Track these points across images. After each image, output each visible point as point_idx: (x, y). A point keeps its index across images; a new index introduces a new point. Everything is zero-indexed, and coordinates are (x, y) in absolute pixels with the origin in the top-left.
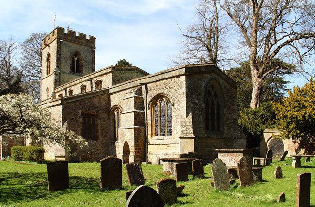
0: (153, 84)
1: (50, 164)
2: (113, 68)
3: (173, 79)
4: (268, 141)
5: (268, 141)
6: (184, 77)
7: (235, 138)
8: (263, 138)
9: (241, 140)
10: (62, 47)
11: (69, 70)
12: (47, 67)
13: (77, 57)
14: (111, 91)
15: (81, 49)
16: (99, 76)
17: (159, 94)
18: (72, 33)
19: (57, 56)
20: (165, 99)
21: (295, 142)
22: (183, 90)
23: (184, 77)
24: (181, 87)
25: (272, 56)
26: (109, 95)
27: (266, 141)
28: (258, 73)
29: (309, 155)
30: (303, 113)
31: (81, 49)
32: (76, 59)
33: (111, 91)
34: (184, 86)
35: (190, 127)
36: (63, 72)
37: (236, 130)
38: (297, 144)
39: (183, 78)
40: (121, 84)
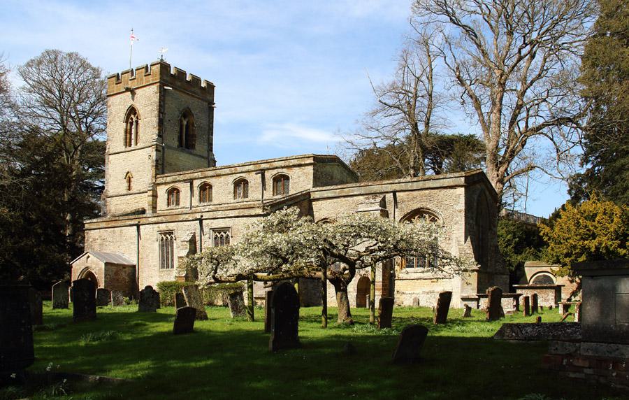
0: (407, 193)
2: (316, 158)
3: (443, 191)
4: (531, 278)
5: (531, 278)
6: (463, 189)
7: (496, 273)
8: (524, 274)
9: (505, 276)
11: (176, 143)
12: (126, 132)
13: (187, 120)
14: (313, 196)
15: (195, 104)
16: (282, 167)
17: (419, 209)
19: (159, 116)
20: (427, 216)
21: (572, 282)
22: (461, 205)
23: (463, 189)
24: (457, 202)
25: (518, 150)
26: (311, 201)
27: (528, 278)
28: (498, 175)
29: (367, 302)
30: (596, 242)
31: (195, 104)
32: (185, 123)
33: (313, 196)
34: (462, 200)
35: (471, 256)
36: (169, 147)
37: (496, 262)
38: (575, 284)
39: (461, 191)
40: (339, 187)
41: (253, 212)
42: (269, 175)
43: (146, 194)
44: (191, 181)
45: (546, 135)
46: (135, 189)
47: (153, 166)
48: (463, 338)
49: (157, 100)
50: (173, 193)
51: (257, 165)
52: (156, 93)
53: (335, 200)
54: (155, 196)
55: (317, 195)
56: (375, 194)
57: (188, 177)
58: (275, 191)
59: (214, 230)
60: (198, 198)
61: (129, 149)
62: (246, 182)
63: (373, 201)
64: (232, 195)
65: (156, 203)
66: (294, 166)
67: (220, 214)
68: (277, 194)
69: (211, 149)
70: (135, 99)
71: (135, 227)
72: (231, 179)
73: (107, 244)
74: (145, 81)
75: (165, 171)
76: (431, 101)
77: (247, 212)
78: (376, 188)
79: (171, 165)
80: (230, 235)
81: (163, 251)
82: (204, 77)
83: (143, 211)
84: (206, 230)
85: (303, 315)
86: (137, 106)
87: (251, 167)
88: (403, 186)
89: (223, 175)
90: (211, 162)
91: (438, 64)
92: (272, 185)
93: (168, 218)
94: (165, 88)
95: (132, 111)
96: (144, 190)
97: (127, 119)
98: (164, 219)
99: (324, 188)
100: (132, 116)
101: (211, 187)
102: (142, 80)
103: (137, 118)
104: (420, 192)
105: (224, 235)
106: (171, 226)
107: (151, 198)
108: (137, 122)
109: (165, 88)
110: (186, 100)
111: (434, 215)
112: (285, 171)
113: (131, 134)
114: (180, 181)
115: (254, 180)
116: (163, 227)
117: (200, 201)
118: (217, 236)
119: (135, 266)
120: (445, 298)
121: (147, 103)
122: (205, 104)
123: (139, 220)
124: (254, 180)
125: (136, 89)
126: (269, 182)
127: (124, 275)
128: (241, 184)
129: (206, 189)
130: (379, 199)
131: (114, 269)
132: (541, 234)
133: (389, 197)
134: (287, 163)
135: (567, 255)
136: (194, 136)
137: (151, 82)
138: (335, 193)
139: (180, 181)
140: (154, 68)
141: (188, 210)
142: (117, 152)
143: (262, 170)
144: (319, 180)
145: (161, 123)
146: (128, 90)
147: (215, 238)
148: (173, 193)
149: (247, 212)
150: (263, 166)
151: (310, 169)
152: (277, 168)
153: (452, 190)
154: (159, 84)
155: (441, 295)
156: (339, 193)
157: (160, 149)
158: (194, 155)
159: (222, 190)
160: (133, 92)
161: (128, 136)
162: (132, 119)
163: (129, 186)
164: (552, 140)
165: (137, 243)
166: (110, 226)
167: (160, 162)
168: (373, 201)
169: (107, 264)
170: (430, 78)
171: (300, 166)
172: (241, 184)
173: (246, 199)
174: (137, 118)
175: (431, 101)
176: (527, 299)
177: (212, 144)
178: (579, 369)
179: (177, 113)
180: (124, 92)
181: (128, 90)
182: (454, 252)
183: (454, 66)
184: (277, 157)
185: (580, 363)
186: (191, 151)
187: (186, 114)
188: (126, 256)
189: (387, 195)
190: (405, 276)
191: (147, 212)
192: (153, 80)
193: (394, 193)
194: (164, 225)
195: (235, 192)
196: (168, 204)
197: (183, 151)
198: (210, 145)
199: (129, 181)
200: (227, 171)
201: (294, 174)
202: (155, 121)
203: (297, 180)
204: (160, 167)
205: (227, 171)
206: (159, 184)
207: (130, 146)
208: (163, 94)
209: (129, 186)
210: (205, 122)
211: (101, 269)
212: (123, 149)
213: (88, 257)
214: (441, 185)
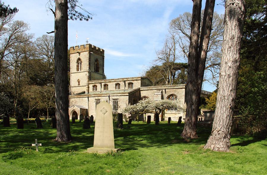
1: (252, 20)
3: (179, 89)
6: (185, 89)
10: (91, 56)
11: (94, 70)
12: (77, 66)
17: (172, 94)
18: (95, 47)
19: (89, 62)
20: (174, 96)
23: (185, 89)
32: (96, 63)
41: (125, 94)
43: (86, 87)
44: (101, 83)
45: (210, 70)
46: (81, 85)
49: (88, 56)
50: (95, 87)
53: (147, 91)
54: (88, 87)
56: (159, 90)
57: (100, 82)
58: (129, 87)
59: (113, 99)
60: (103, 88)
61: (78, 72)
62: (119, 84)
63: (159, 92)
65: (89, 90)
66: (135, 80)
67: (115, 95)
69: (103, 72)
75: (91, 80)
76: (174, 57)
77: (124, 95)
78: (160, 88)
79: (92, 77)
80: (118, 101)
82: (101, 48)
83: (84, 92)
84: (111, 99)
86: (81, 58)
87: (121, 80)
88: (168, 88)
90: (104, 77)
91: (177, 46)
93: (98, 96)
95: (79, 59)
96: (85, 85)
97: (77, 62)
98: (97, 96)
99: (144, 87)
100: (79, 61)
101: (108, 85)
102: (82, 49)
103: (81, 62)
104: (173, 89)
106: (99, 98)
107: (87, 88)
108: (81, 63)
110: (97, 56)
112: (132, 82)
113: (79, 67)
114: (97, 83)
115: (122, 84)
116: (97, 98)
117: (104, 89)
119: (87, 109)
120: (180, 118)
121: (85, 57)
124: (122, 84)
126: (127, 85)
127: (85, 112)
128: (118, 85)
129: (106, 86)
130: (161, 91)
131: (82, 110)
132: (206, 101)
133: (164, 90)
134: (132, 79)
135: (213, 107)
136: (99, 68)
139: (97, 83)
140: (87, 46)
143: (124, 81)
144: (143, 85)
145: (90, 64)
146: (78, 52)
148: (95, 87)
149: (124, 95)
150: (125, 80)
151: (140, 81)
152: (129, 80)
153: (182, 89)
155: (180, 117)
157: (90, 72)
158: (99, 74)
159: (112, 86)
160: (79, 53)
162: (79, 62)
163: (79, 84)
164: (211, 71)
167: (90, 77)
168: (159, 92)
169: (80, 109)
170: (174, 50)
171: (137, 80)
172: (118, 85)
173: (119, 89)
174: (81, 62)
175: (174, 57)
176: (200, 119)
177: (104, 70)
178: (202, 125)
179: (94, 60)
182: (182, 106)
183: (182, 47)
184: (129, 77)
185: (203, 125)
187: (97, 60)
188: (84, 106)
190: (167, 113)
191: (86, 92)
193: (165, 89)
195: (116, 87)
196: (93, 90)
197: (96, 73)
199: (79, 82)
200: (113, 81)
201: (134, 82)
202: (88, 63)
204: (90, 78)
205: (113, 81)
207: (78, 71)
208: (90, 54)
209: (79, 84)
210: (102, 63)
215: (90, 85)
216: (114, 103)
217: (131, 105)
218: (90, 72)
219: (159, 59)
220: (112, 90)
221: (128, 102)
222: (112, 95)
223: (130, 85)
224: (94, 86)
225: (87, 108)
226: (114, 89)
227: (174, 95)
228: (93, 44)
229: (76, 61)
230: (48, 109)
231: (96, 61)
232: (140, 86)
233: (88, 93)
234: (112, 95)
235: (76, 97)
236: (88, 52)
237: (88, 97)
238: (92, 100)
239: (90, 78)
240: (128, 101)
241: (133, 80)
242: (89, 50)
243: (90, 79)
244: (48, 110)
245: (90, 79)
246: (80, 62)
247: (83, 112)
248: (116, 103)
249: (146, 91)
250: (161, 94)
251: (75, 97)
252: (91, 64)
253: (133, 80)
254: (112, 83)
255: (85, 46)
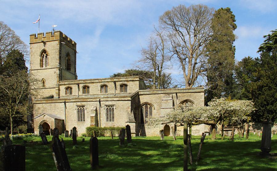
3: (196, 93)
11: (65, 68)
12: (41, 61)
16: (124, 81)
17: (187, 100)
18: (66, 37)
26: (139, 95)
41: (126, 99)
42: (81, 86)
46: (47, 85)
47: (57, 77)
48: (249, 142)
50: (69, 89)
51: (112, 80)
52: (58, 45)
53: (150, 95)
54: (59, 90)
55: (142, 93)
56: (168, 94)
58: (121, 91)
59: (106, 106)
60: (82, 92)
61: (42, 68)
64: (100, 91)
65: (60, 92)
66: (130, 81)
67: (109, 99)
68: (121, 92)
69: (75, 71)
70: (46, 46)
71: (64, 103)
72: (99, 85)
73: (47, 110)
74: (51, 39)
77: (123, 99)
81: (78, 114)
82: (74, 40)
83: (52, 97)
85: (196, 135)
88: (180, 91)
89: (95, 83)
92: (119, 88)
93: (82, 100)
94: (62, 43)
95: (44, 51)
96: (54, 87)
98: (79, 100)
100: (44, 54)
101: (88, 87)
102: (49, 38)
103: (47, 55)
104: (187, 93)
105: (112, 108)
106: (83, 103)
108: (46, 57)
109: (62, 43)
111: (192, 102)
112: (126, 83)
114: (72, 84)
116: (79, 104)
118: (108, 108)
122: (74, 51)
123: (65, 100)
124: (111, 85)
125: (47, 42)
127: (60, 124)
130: (171, 96)
137: (54, 40)
138: (150, 92)
139: (72, 84)
140: (56, 33)
141: (77, 97)
142: (36, 69)
143: (78, 84)
145: (60, 58)
146: (42, 42)
147: (107, 109)
148: (69, 89)
149: (123, 99)
151: (138, 82)
152: (122, 81)
154: (59, 41)
156: (152, 92)
157: (60, 69)
158: (70, 73)
160: (44, 43)
161: (42, 62)
162: (44, 55)
165: (65, 110)
166: (48, 102)
167: (60, 75)
173: (107, 93)
174: (47, 55)
180: (41, 42)
181: (42, 42)
184: (87, 79)
186: (69, 71)
187: (68, 55)
189: (173, 94)
192: (56, 39)
193: (176, 93)
194: (80, 103)
195: (101, 90)
196: (66, 94)
198: (75, 69)
200: (97, 81)
202: (57, 57)
203: (131, 87)
205: (97, 81)
206: (61, 85)
207: (43, 67)
210: (74, 59)
211: (52, 121)
212: (40, 68)
213: (45, 116)
214: (195, 91)
215: (60, 87)
216: (107, 111)
217: (206, 106)
218: (60, 69)
219: (146, 58)
220: (95, 94)
221: (130, 110)
222: (105, 99)
223: (122, 88)
224: (67, 89)
225: (63, 119)
226: (99, 92)
227: (189, 101)
228: (65, 33)
229: (39, 53)
230: (13, 118)
231: (67, 56)
232: (138, 89)
233: (59, 98)
234: (105, 99)
235: (44, 102)
236: (58, 41)
237: (65, 103)
238: (72, 107)
239: (60, 77)
240: (130, 108)
241: (127, 81)
242: (60, 38)
243: (61, 78)
244: (11, 120)
245: (61, 78)
246: (45, 55)
247: (58, 123)
248: (110, 111)
249: (147, 95)
250: (171, 99)
251: (43, 102)
252: (61, 58)
253: (127, 81)
254: (95, 84)
255: (37, 36)
